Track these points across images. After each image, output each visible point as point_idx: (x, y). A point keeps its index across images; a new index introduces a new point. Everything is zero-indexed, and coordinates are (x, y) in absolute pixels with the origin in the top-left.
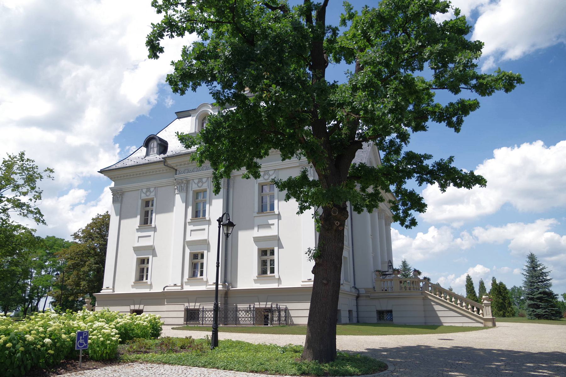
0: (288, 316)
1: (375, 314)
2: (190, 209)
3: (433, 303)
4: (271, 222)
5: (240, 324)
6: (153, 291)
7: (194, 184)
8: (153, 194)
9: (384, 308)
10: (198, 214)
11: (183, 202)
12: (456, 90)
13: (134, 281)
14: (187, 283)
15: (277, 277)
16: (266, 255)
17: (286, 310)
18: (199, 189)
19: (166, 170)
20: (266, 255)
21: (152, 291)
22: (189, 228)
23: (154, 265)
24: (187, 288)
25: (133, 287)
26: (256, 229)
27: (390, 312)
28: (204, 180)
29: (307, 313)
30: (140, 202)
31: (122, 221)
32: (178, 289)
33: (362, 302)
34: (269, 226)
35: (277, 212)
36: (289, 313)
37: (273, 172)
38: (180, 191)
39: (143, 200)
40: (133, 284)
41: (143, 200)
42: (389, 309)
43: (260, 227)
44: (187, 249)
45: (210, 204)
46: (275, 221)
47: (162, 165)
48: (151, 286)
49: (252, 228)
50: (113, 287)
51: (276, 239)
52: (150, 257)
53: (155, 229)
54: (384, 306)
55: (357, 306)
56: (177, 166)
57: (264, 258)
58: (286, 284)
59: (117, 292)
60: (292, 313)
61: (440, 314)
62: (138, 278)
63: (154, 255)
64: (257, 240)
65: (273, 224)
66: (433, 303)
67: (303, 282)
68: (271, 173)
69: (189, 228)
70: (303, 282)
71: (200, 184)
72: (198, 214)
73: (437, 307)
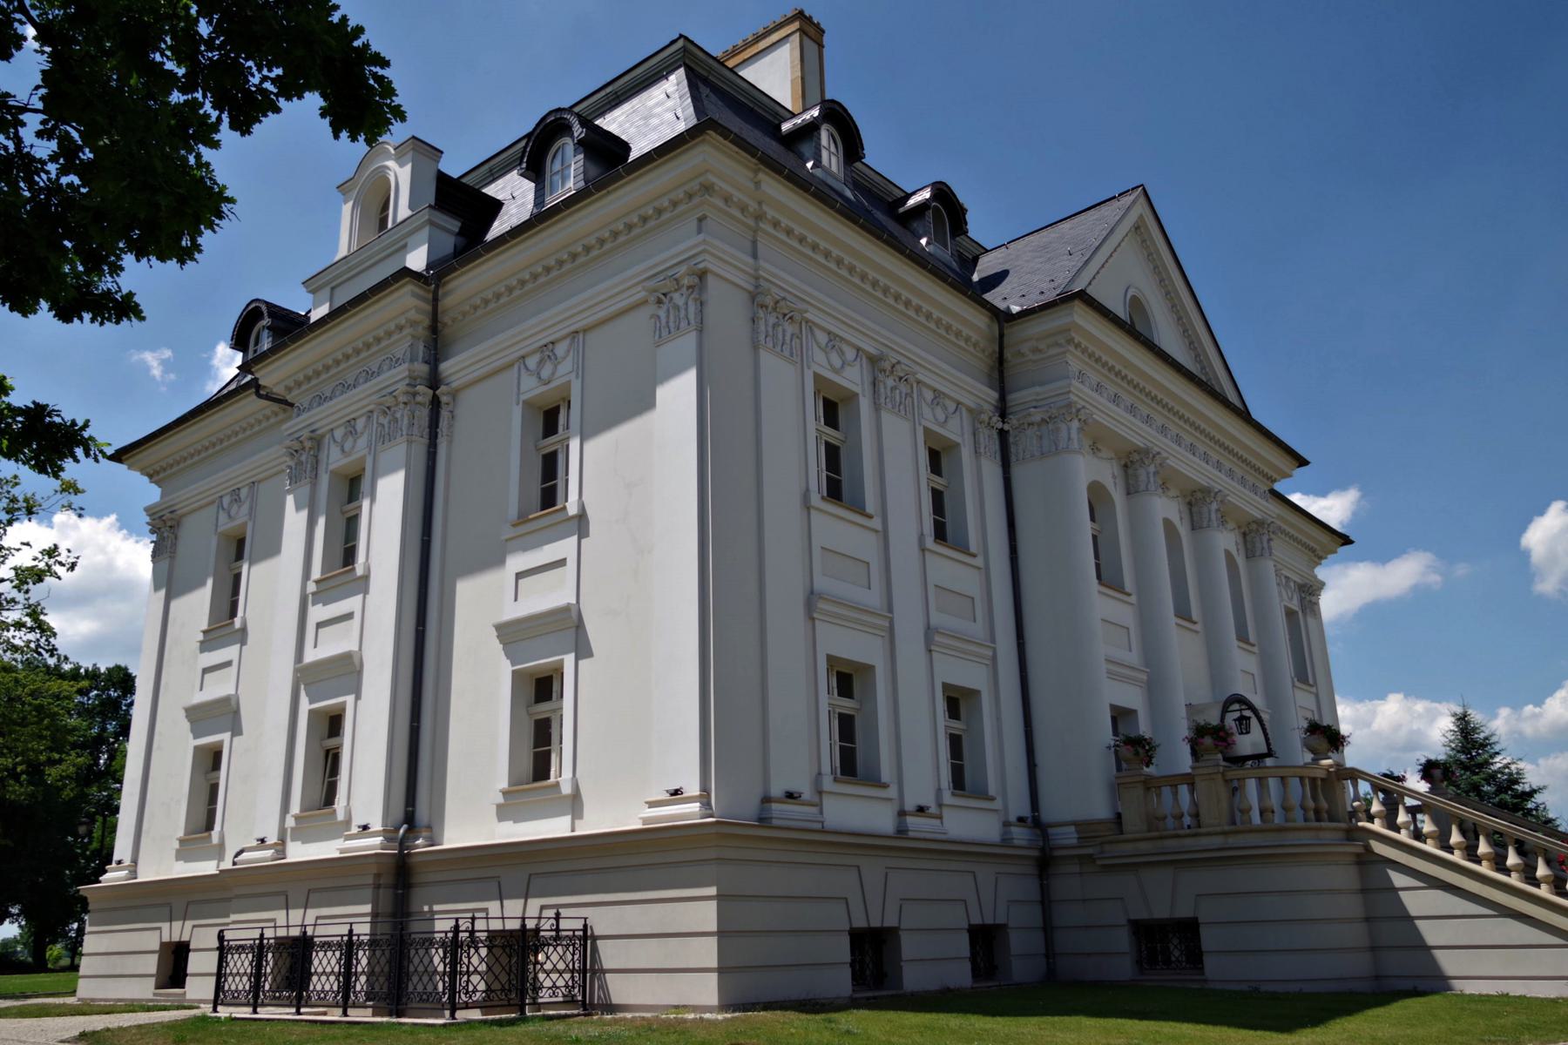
0: (588, 970)
1: (1123, 940)
5: (537, 1006)
6: (592, 824)
7: (333, 446)
8: (565, 367)
9: (1161, 911)
12: (265, 329)
13: (504, 784)
17: (586, 939)
18: (345, 461)
21: (581, 831)
23: (587, 695)
24: (298, 852)
27: (1189, 929)
29: (707, 952)
30: (517, 412)
33: (1067, 884)
35: (572, 509)
36: (595, 950)
37: (566, 343)
39: (528, 405)
40: (500, 799)
41: (528, 405)
42: (1184, 911)
48: (574, 804)
50: (135, 861)
52: (569, 660)
53: (581, 524)
54: (1164, 898)
55: (1046, 902)
56: (289, 389)
60: (610, 955)
61: (1432, 933)
62: (527, 764)
63: (583, 649)
66: (1398, 879)
67: (652, 804)
73: (1418, 901)
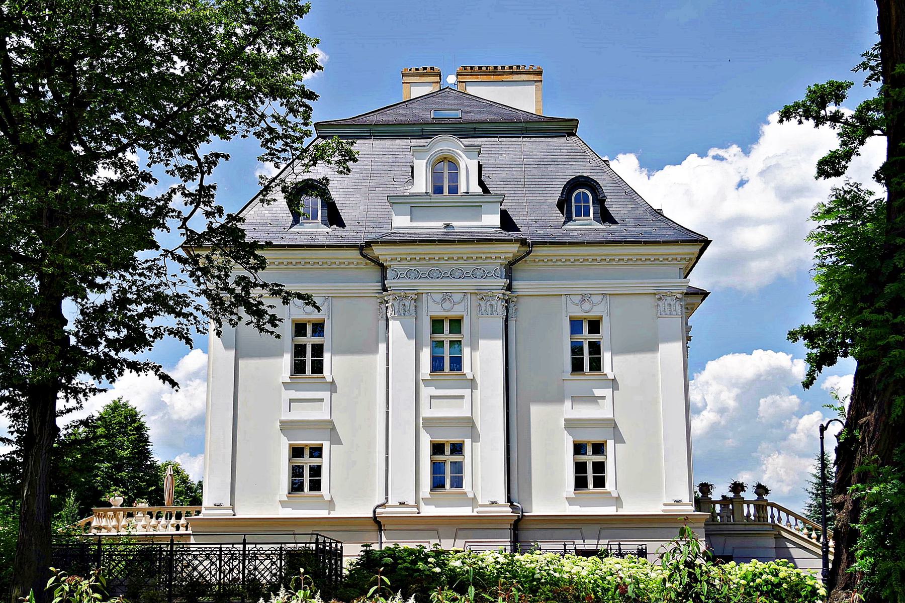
2: (426, 355)
3: (789, 545)
4: (598, 392)
10: (447, 364)
11: (409, 337)
14: (427, 502)
15: (327, 498)
16: (443, 452)
19: (366, 264)
20: (443, 452)
21: (333, 515)
22: (426, 392)
24: (428, 511)
25: (283, 504)
26: (568, 404)
28: (457, 297)
31: (242, 363)
32: (226, 513)
34: (594, 400)
38: (401, 314)
43: (575, 399)
44: (423, 433)
45: (474, 347)
46: (607, 392)
47: (356, 253)
49: (560, 400)
51: (329, 429)
57: (298, 462)
58: (629, 509)
59: (243, 513)
64: (570, 425)
65: (603, 398)
66: (789, 545)
67: (665, 505)
68: (595, 299)
69: (426, 392)
70: (665, 505)
71: (447, 305)
72: (447, 364)
